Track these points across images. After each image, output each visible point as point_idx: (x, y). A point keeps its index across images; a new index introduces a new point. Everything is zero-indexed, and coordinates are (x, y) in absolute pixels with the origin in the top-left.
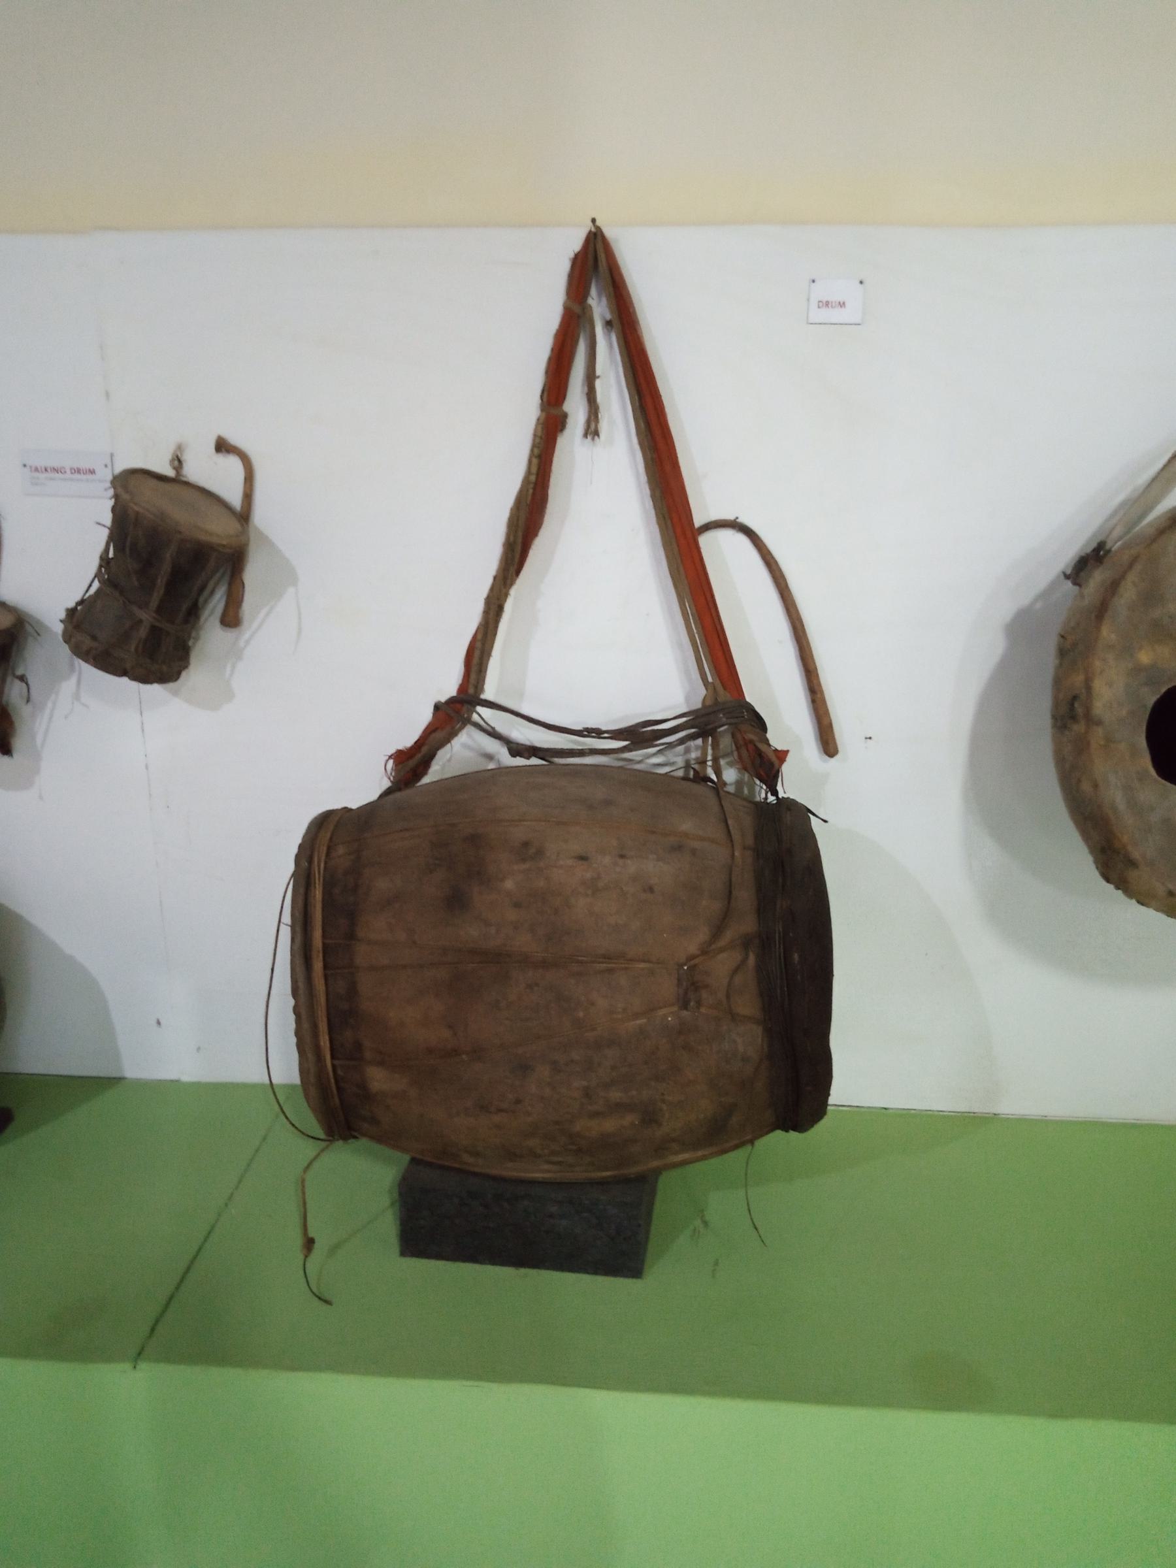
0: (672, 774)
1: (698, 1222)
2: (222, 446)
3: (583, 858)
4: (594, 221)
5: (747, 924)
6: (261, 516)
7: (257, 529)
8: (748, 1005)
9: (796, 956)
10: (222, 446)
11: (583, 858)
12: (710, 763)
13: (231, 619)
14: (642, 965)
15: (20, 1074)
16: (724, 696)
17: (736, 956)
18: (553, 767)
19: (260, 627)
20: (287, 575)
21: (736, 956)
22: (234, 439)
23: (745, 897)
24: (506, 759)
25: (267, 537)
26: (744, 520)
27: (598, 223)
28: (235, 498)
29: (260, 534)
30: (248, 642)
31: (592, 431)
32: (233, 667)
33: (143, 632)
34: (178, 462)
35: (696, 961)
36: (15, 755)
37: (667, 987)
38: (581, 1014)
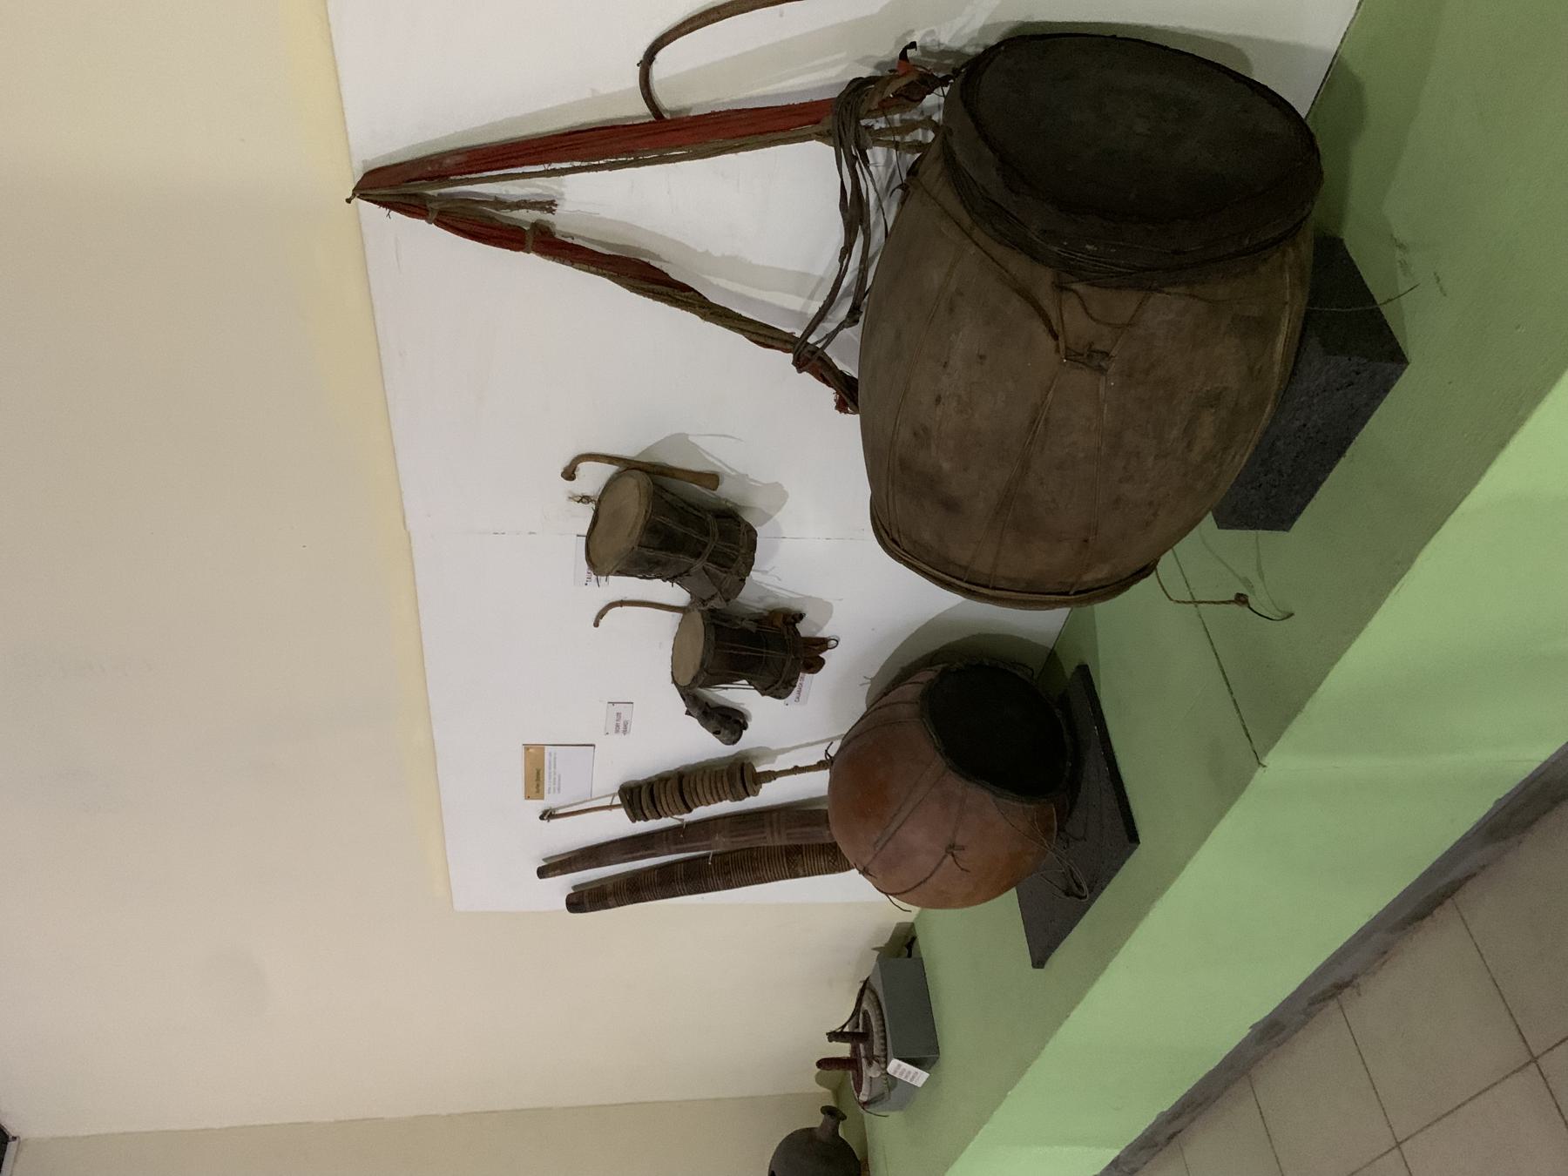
0: (890, 226)
1: (1398, 253)
2: (569, 474)
3: (938, 400)
4: (349, 201)
5: (1042, 279)
6: (629, 450)
7: (638, 456)
8: (1125, 303)
9: (1089, 247)
10: (569, 474)
11: (938, 400)
12: (898, 138)
13: (712, 479)
14: (1050, 396)
15: (1060, 633)
16: (828, 123)
17: (1071, 303)
18: (873, 291)
19: (720, 461)
20: (681, 439)
21: (1071, 303)
22: (565, 461)
23: (1018, 265)
24: (858, 328)
25: (648, 449)
26: (640, 56)
27: (349, 195)
28: (610, 470)
29: (642, 453)
30: (732, 470)
31: (549, 205)
32: (752, 480)
33: (712, 567)
34: (584, 499)
35: (1062, 346)
36: (804, 611)
37: (1081, 378)
38: (1081, 455)
